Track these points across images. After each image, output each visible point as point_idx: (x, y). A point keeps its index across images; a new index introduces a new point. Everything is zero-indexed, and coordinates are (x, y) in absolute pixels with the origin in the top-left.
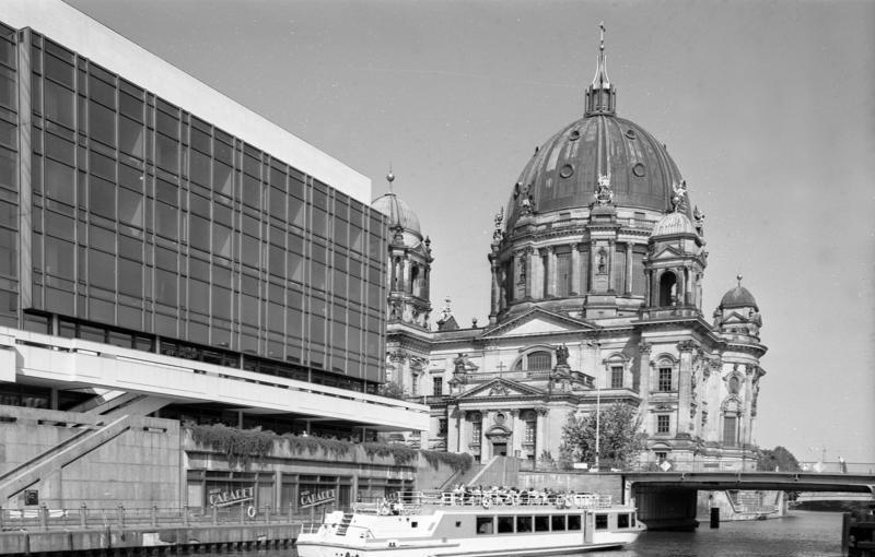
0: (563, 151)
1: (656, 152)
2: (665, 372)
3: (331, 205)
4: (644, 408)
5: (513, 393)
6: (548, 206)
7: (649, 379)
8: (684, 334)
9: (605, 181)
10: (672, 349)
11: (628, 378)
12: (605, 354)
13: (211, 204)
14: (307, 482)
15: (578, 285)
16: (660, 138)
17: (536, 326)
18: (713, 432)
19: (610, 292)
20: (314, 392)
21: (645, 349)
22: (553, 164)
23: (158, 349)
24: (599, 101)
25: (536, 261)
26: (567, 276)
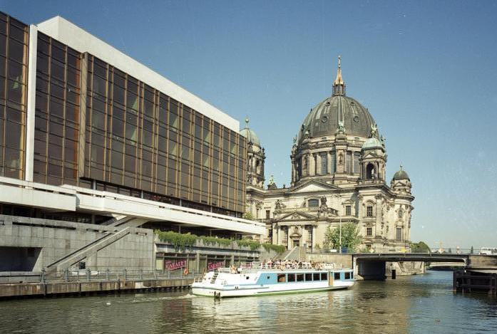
0: (323, 111)
1: (364, 112)
2: (370, 208)
5: (302, 218)
6: (316, 134)
7: (363, 211)
8: (378, 191)
9: (341, 124)
10: (372, 198)
12: (343, 200)
15: (330, 169)
16: (366, 106)
19: (345, 173)
21: (361, 198)
22: (318, 116)
24: (338, 89)
25: (311, 159)
26: (325, 165)
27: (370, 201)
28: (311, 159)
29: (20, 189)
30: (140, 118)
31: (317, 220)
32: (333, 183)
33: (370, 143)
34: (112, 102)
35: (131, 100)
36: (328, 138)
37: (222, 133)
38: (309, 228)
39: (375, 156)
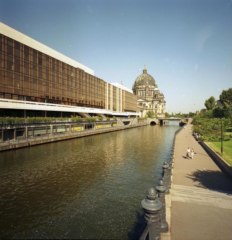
0: (142, 78)
1: (152, 78)
2: (156, 106)
3: (96, 80)
4: (154, 110)
5: (139, 109)
6: (140, 85)
7: (154, 107)
8: (158, 102)
9: (147, 83)
10: (157, 103)
11: (152, 106)
12: (149, 104)
13: (56, 73)
14: (30, 129)
15: (144, 95)
16: (153, 76)
17: (140, 100)
18: (161, 112)
19: (148, 96)
20: (26, 103)
21: (154, 103)
22: (140, 80)
23: (25, 99)
24: (145, 71)
25: (139, 92)
26: (143, 93)
27: (156, 104)
28: (139, 92)
29: (74, 108)
30: (44, 69)
31: (144, 109)
32: (145, 99)
33: (156, 89)
34: (51, 70)
35: (83, 78)
36: (144, 86)
37: (96, 80)
38: (142, 111)
39: (157, 93)
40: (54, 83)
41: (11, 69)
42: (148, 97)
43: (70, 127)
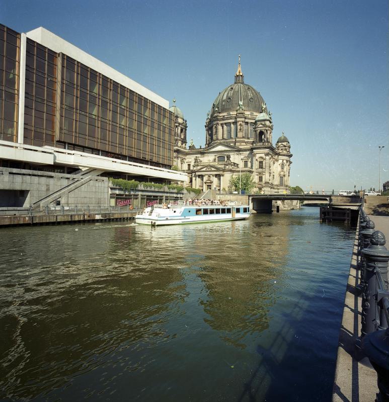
0: (228, 94)
2: (261, 163)
4: (254, 174)
5: (213, 169)
6: (223, 110)
7: (256, 165)
8: (267, 151)
9: (241, 103)
10: (263, 155)
12: (242, 157)
15: (233, 135)
16: (258, 90)
18: (276, 182)
19: (243, 137)
21: (254, 155)
22: (225, 98)
24: (238, 79)
25: (220, 127)
26: (229, 132)
27: (261, 158)
28: (220, 127)
29: (14, 149)
31: (224, 171)
37: (156, 109)
39: (265, 125)
40: (139, 132)
41: (15, 87)
42: (243, 142)
43: (140, 198)
